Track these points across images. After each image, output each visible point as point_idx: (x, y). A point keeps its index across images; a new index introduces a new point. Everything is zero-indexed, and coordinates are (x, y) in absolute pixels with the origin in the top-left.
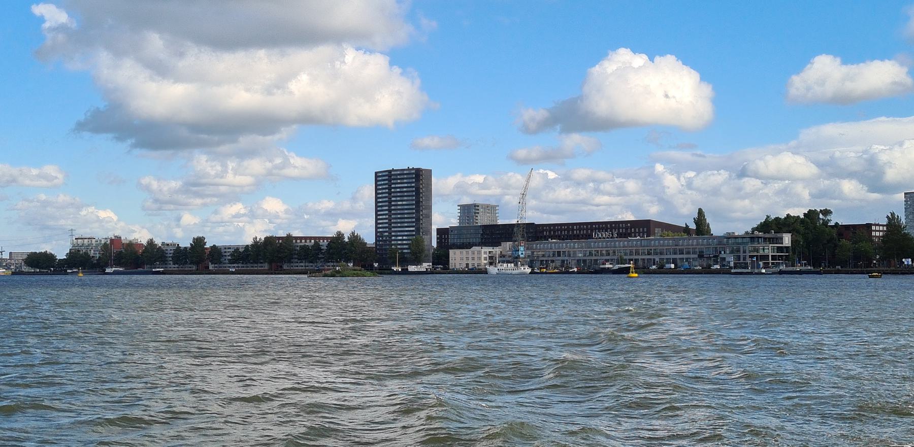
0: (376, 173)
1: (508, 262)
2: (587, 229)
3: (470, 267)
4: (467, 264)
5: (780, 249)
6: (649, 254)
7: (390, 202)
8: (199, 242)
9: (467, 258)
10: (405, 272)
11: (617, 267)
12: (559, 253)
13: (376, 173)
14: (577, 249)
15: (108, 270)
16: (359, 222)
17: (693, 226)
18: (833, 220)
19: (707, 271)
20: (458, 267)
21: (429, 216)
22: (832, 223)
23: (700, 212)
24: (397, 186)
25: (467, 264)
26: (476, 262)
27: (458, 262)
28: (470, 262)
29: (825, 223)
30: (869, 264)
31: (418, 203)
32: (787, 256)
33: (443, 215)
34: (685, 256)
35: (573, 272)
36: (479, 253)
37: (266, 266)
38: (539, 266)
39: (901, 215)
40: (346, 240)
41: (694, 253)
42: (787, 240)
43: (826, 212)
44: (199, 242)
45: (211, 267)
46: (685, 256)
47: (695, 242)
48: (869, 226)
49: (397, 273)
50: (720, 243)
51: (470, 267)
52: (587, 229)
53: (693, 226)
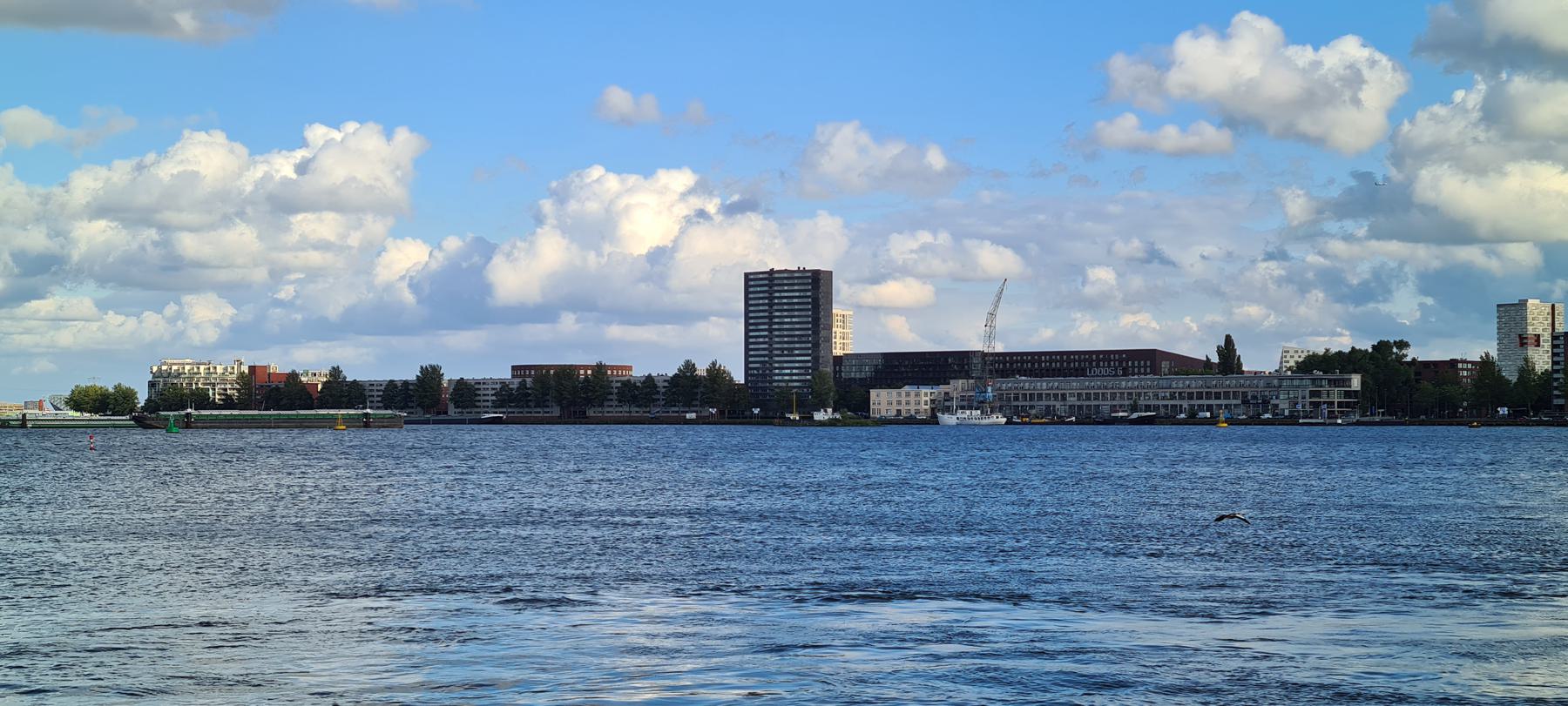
0: (746, 275)
1: (971, 408)
2: (1062, 362)
3: (904, 414)
4: (899, 411)
5: (1348, 394)
6: (1173, 397)
7: (771, 318)
8: (431, 375)
9: (899, 403)
10: (808, 420)
11: (1135, 415)
12: (1040, 395)
13: (746, 275)
14: (1073, 386)
15: (819, 416)
16: (722, 346)
17: (1215, 359)
18: (1411, 354)
19: (1255, 420)
20: (883, 413)
21: (829, 340)
22: (1409, 359)
23: (1228, 339)
24: (783, 294)
25: (899, 411)
26: (913, 408)
27: (883, 407)
28: (903, 408)
29: (1400, 358)
30: (1454, 414)
31: (816, 321)
32: (1353, 403)
33: (852, 335)
34: (1223, 402)
35: (1071, 423)
36: (917, 395)
37: (556, 411)
38: (1018, 413)
39: (1494, 354)
40: (739, 377)
41: (1235, 395)
42: (1356, 382)
43: (1402, 345)
44: (431, 375)
45: (590, 413)
46: (1223, 402)
47: (1216, 382)
48: (1454, 362)
49: (793, 423)
50: (1268, 385)
51: (904, 414)
52: (1062, 362)
53: (1215, 359)
